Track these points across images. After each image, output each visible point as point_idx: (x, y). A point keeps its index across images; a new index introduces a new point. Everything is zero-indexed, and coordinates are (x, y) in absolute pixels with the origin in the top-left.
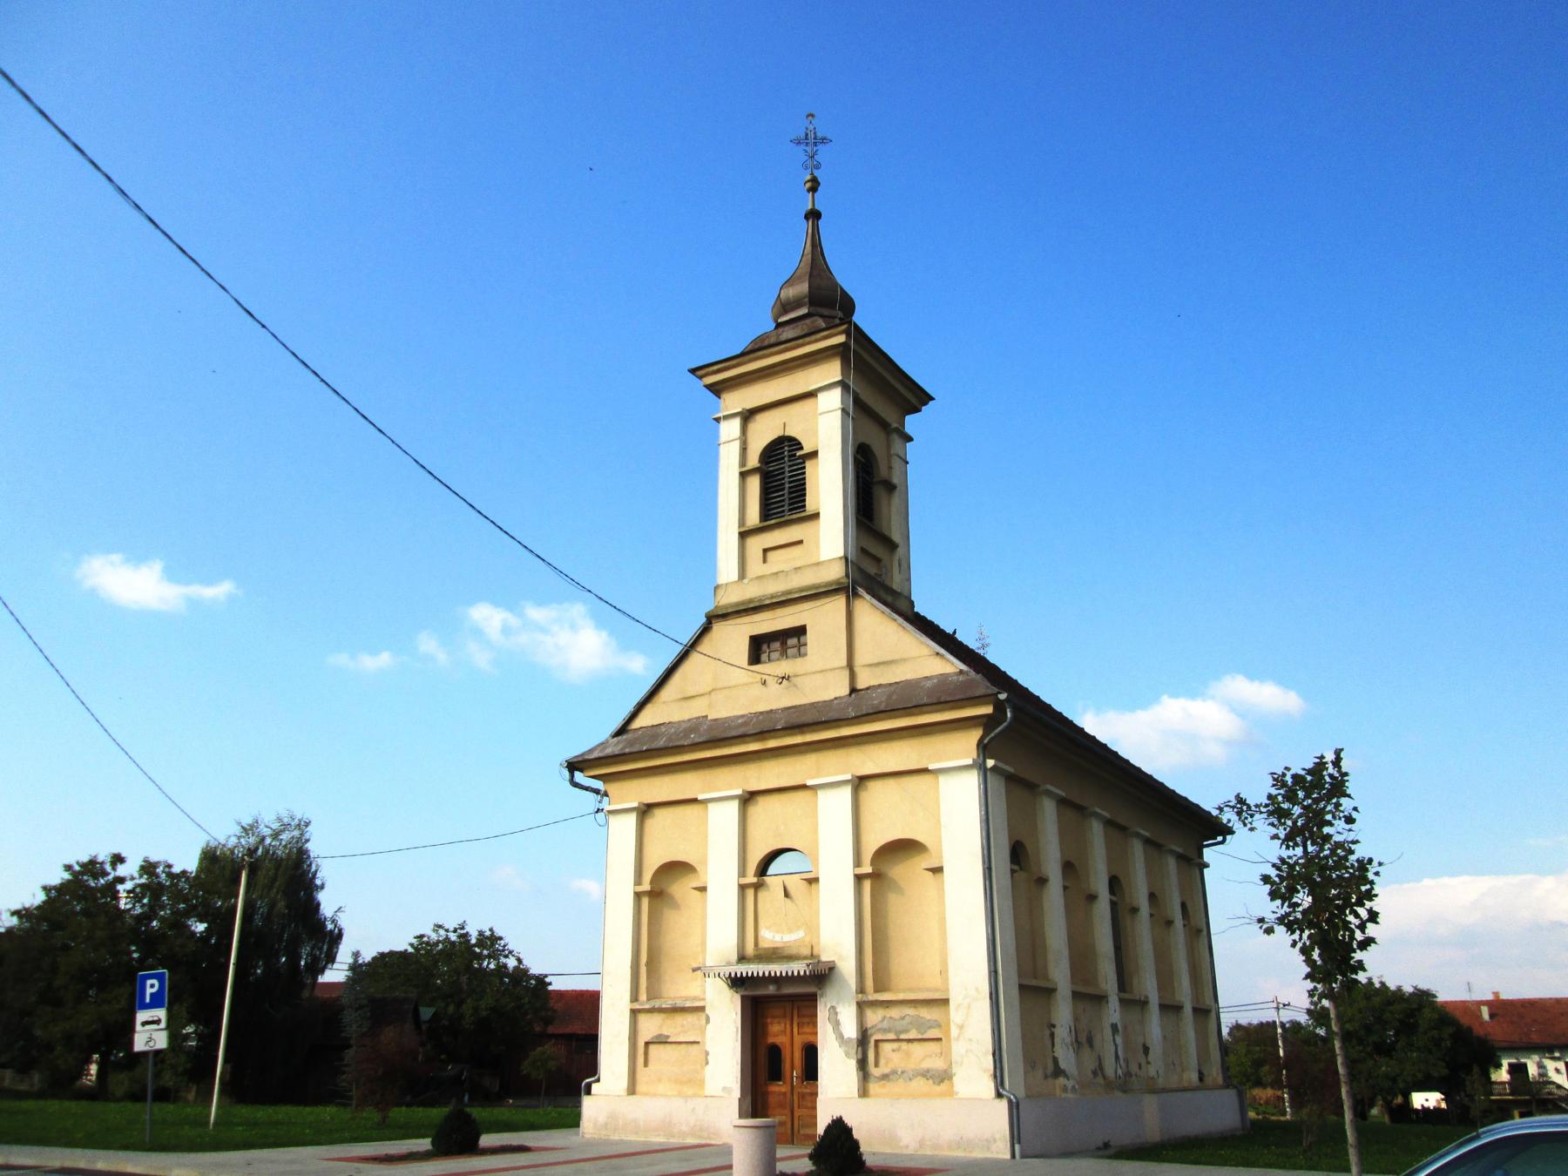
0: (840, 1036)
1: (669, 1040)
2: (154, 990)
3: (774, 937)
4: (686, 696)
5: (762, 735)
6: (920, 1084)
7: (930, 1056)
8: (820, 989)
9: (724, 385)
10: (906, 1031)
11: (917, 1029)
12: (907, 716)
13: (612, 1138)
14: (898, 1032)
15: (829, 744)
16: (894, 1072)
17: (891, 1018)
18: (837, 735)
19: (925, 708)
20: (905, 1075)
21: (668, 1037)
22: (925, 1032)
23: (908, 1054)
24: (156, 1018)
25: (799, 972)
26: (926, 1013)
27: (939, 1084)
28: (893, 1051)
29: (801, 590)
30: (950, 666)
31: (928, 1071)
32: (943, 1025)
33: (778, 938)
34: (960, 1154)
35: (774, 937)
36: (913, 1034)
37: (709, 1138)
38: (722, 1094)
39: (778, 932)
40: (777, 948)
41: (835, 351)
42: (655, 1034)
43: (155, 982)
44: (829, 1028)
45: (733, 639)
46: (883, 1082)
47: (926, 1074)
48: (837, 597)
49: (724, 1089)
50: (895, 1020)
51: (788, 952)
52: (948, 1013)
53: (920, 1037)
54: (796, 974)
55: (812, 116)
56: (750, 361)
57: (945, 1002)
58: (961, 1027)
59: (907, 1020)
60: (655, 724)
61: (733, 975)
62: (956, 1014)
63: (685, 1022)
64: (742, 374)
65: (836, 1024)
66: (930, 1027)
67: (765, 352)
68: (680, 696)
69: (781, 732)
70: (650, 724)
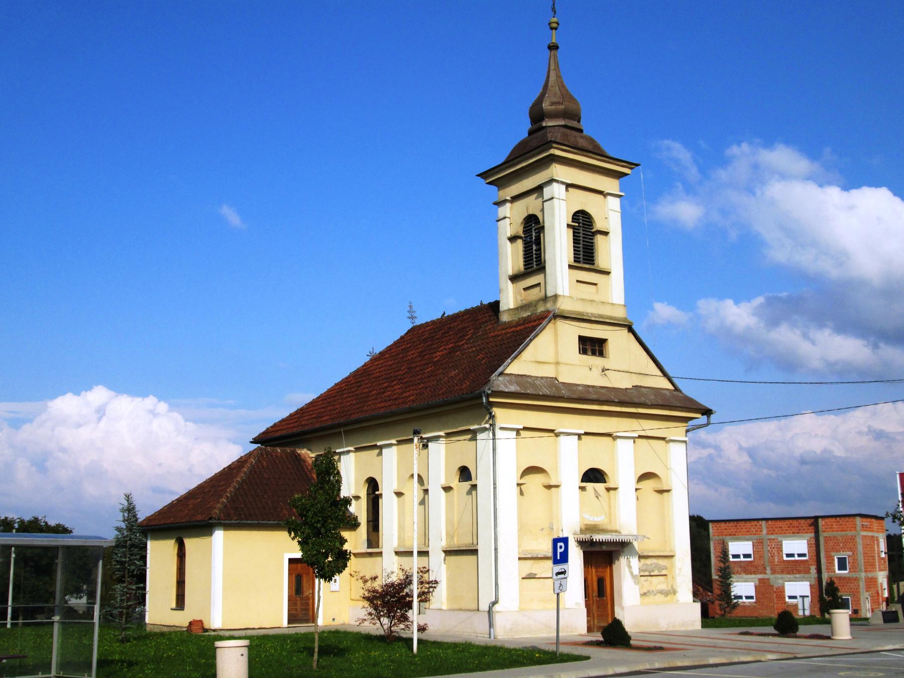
0: (632, 573)
1: (536, 577)
2: (562, 550)
5: (622, 403)
6: (660, 597)
7: (660, 583)
10: (653, 571)
11: (658, 570)
13: (515, 637)
14: (650, 572)
15: (660, 418)
16: (649, 592)
17: (646, 564)
18: (637, 412)
19: (678, 408)
20: (653, 593)
21: (536, 574)
22: (661, 571)
23: (651, 582)
24: (563, 570)
26: (662, 562)
28: (645, 581)
29: (611, 318)
31: (662, 590)
32: (668, 568)
34: (683, 629)
36: (656, 573)
37: (571, 632)
38: (575, 607)
40: (597, 525)
42: (528, 573)
43: (562, 544)
44: (627, 569)
45: (570, 333)
46: (644, 597)
47: (661, 592)
48: (623, 329)
49: (576, 604)
50: (649, 565)
51: (601, 527)
52: (413, 559)
53: (659, 574)
58: (680, 569)
59: (653, 566)
60: (520, 374)
61: (579, 540)
63: (545, 566)
65: (630, 567)
66: (663, 569)
67: (593, 156)
68: (534, 360)
69: (616, 404)
70: (517, 374)
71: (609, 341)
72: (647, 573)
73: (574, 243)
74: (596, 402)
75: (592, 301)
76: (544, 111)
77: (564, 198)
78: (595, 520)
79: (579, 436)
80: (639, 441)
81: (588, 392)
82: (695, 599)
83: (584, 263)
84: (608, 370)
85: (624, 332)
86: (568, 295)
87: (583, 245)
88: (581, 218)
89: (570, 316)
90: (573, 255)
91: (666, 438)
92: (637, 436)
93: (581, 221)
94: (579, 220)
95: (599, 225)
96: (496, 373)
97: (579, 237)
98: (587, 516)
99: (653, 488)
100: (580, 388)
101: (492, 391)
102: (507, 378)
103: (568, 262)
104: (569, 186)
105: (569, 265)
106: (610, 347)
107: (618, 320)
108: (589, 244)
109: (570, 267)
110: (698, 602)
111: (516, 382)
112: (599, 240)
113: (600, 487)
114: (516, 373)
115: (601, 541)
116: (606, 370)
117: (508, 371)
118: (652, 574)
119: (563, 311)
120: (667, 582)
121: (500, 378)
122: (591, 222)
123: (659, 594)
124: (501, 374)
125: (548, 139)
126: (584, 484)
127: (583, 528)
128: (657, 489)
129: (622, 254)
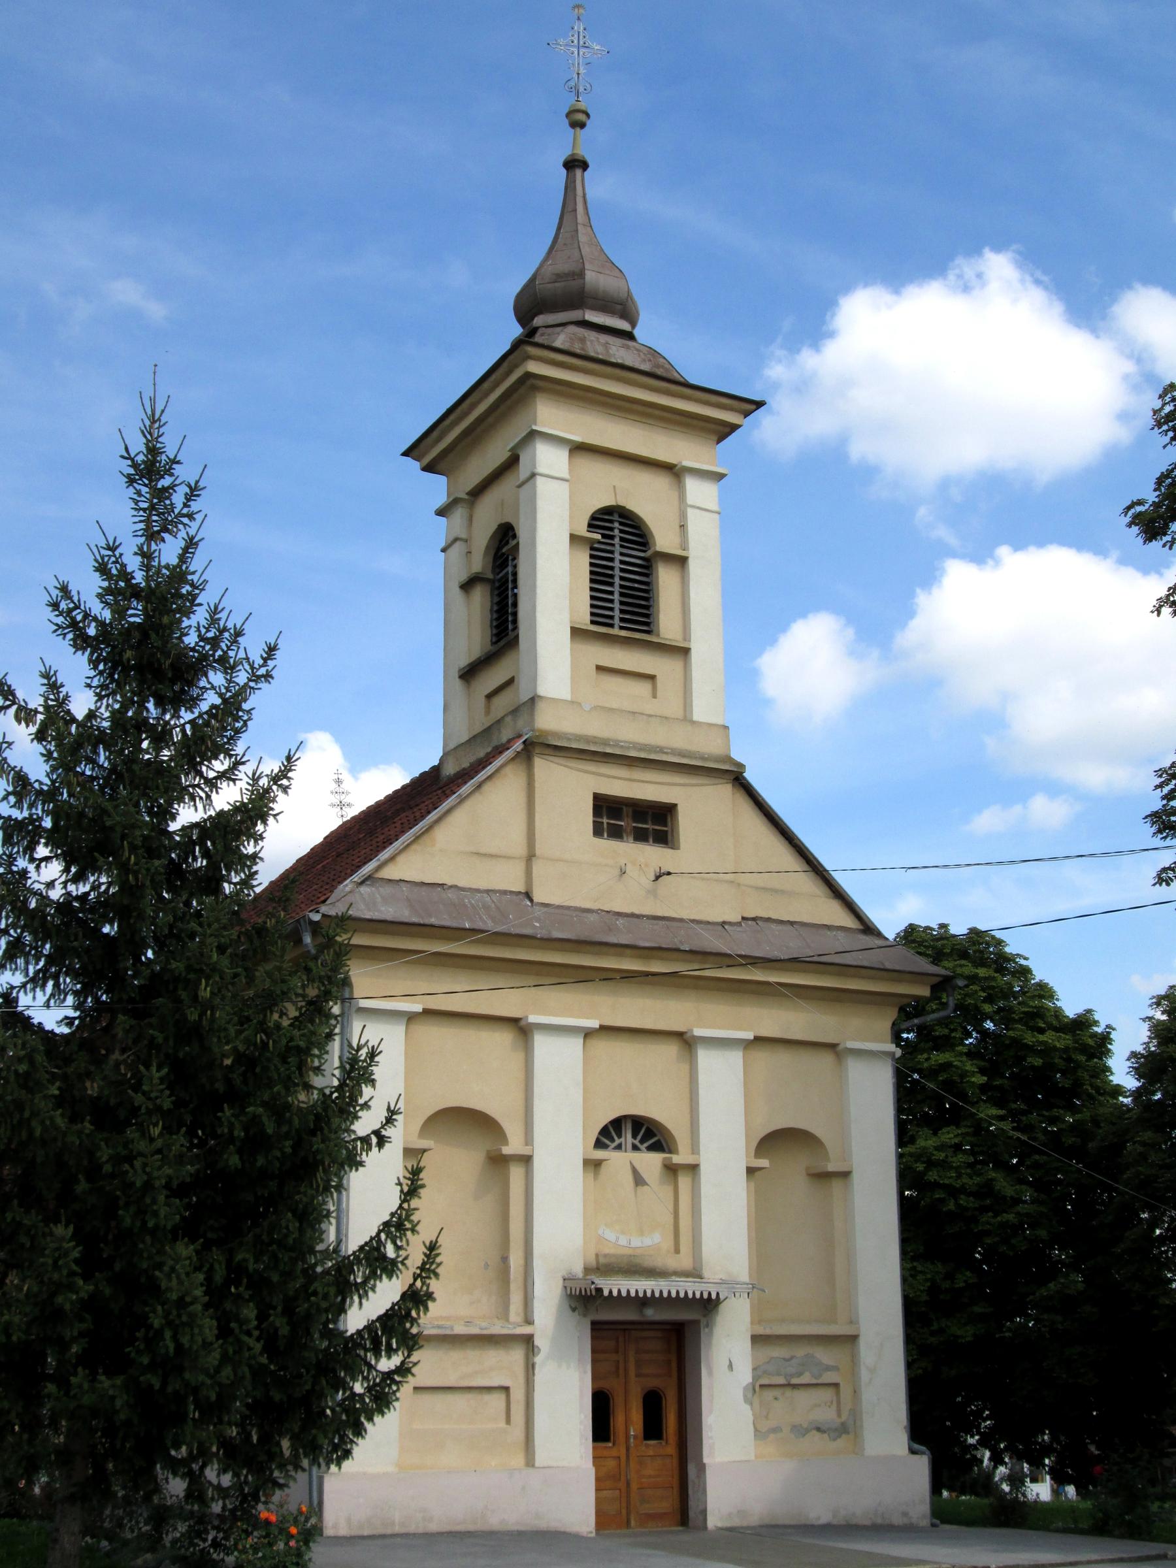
3: (618, 1238)
4: (483, 851)
8: (705, 1316)
9: (550, 386)
10: (800, 1374)
12: (805, 972)
25: (694, 1294)
27: (835, 1440)
29: (682, 754)
30: (849, 922)
33: (636, 1242)
35: (618, 1238)
36: (806, 1379)
39: (623, 1233)
41: (713, 426)
53: (814, 1381)
54: (690, 1296)
55: (578, 6)
56: (619, 379)
57: (853, 1339)
62: (866, 1353)
64: (611, 393)
71: (680, 808)
72: (781, 1381)
73: (592, 581)
74: (628, 951)
75: (634, 713)
76: (586, 289)
77: (566, 475)
78: (633, 1245)
79: (588, 1034)
80: (604, 1047)
81: (610, 929)
82: (916, 1446)
83: (621, 628)
84: (669, 873)
85: (725, 791)
86: (568, 697)
87: (622, 586)
88: (616, 525)
89: (566, 745)
90: (587, 601)
91: (838, 1044)
92: (752, 1038)
93: (616, 532)
94: (612, 529)
95: (664, 540)
96: (356, 877)
97: (612, 568)
98: (610, 1235)
99: (807, 1168)
100: (592, 918)
101: (324, 916)
102: (387, 890)
103: (571, 622)
104: (579, 449)
105: (571, 628)
106: (686, 823)
107: (703, 758)
108: (636, 585)
109: (577, 633)
110: (923, 1453)
111: (408, 900)
112: (665, 578)
113: (652, 1162)
114: (417, 878)
115: (641, 1295)
116: (664, 874)
117: (390, 872)
118: (794, 1381)
119: (546, 733)
120: (839, 1403)
121: (364, 889)
122: (642, 536)
123: (814, 1432)
124: (368, 879)
125: (554, 342)
126: (600, 1154)
127: (592, 1262)
128: (816, 1171)
129: (539, 591)
